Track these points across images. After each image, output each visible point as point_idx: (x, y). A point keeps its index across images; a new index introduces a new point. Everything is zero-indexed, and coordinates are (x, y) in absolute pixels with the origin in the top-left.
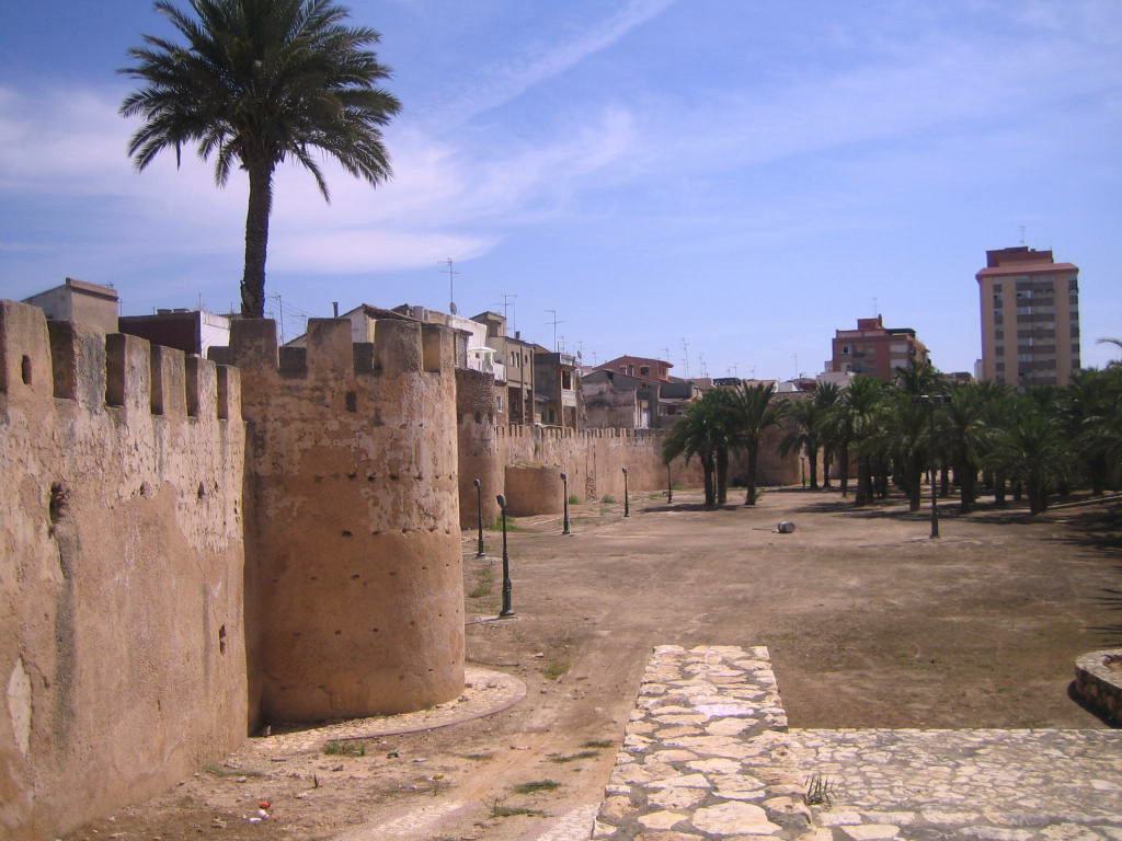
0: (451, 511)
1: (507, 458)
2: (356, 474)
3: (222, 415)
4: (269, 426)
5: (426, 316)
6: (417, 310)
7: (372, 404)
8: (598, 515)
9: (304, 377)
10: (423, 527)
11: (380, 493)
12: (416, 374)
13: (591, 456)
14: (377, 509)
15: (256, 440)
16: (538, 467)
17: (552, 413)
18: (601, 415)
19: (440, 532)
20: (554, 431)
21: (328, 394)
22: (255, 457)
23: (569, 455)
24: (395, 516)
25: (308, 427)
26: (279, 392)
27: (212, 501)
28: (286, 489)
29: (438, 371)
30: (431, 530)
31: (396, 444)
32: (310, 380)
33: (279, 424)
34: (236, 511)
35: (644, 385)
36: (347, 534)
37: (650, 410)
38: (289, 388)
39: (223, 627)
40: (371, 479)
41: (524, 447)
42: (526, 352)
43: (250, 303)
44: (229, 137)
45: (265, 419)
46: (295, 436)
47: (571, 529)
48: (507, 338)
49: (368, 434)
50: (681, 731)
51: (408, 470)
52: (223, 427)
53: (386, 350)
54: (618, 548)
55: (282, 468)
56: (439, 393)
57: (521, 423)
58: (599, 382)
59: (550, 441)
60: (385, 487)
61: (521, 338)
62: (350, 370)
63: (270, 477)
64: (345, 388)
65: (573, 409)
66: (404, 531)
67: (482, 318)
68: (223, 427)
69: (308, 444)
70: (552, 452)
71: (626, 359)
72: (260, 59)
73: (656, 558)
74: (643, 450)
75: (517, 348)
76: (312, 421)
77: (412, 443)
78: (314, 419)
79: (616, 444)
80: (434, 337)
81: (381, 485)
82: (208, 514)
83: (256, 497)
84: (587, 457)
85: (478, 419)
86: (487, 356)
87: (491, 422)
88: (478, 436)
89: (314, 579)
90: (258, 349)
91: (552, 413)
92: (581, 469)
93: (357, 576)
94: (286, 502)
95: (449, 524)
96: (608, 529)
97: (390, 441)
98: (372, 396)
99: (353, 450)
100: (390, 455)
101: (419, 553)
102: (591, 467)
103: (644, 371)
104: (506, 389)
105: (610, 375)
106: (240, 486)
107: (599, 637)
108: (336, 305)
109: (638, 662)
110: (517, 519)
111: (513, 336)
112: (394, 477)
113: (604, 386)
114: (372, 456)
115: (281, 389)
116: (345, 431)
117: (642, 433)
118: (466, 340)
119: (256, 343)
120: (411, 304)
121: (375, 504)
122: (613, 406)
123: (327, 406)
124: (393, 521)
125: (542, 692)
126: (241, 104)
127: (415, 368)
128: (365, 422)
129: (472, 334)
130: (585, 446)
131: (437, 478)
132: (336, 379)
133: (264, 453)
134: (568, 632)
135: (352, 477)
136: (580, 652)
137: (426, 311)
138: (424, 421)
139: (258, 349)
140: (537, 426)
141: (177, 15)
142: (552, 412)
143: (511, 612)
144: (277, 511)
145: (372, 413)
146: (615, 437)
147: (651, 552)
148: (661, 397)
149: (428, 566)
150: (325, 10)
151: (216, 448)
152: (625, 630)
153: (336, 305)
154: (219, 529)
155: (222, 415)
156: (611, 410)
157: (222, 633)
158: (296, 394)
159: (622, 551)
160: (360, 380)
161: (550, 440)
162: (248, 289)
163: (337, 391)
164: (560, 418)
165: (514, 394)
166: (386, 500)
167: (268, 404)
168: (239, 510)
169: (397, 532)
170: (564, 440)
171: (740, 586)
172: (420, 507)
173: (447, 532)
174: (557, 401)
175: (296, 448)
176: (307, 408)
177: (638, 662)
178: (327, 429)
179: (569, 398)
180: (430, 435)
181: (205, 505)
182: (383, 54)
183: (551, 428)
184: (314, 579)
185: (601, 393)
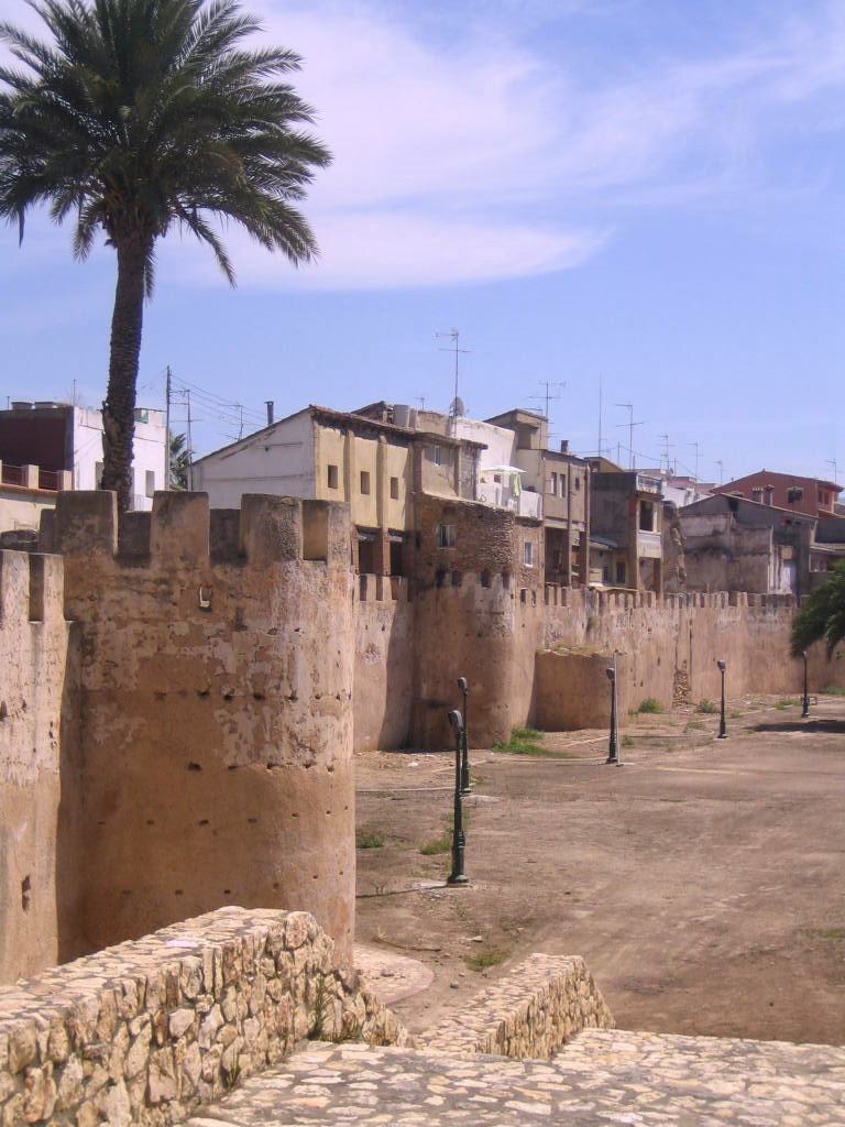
0: (336, 741)
1: (539, 639)
2: (210, 691)
3: (36, 615)
4: (101, 626)
5: (412, 423)
6: (399, 409)
7: (232, 603)
8: (677, 732)
9: (146, 566)
10: (295, 762)
11: (239, 717)
12: (292, 563)
13: (685, 636)
14: (234, 737)
15: (82, 642)
16: (587, 654)
17: (621, 568)
18: (715, 569)
19: (318, 769)
20: (621, 596)
21: (177, 588)
22: (82, 665)
23: (646, 635)
24: (259, 743)
25: (150, 630)
26: (114, 584)
27: (17, 724)
28: (119, 708)
29: (324, 559)
30: (307, 766)
31: (262, 654)
32: (154, 570)
33: (113, 625)
34: (51, 735)
35: (788, 522)
36: (196, 767)
37: (795, 562)
38: (126, 578)
39: (27, 879)
40: (228, 698)
41: (569, 622)
42: (577, 472)
43: (114, 434)
44: (89, 201)
45: (96, 618)
46: (133, 641)
47: (620, 754)
48: (545, 453)
49: (225, 641)
50: (139, 952)
51: (278, 688)
52: (36, 632)
53: (253, 532)
54: (672, 788)
55: (114, 680)
56: (324, 588)
57: (564, 584)
58: (712, 514)
59: (613, 612)
60: (246, 710)
61: (571, 450)
62: (205, 559)
63: (101, 691)
65: (657, 561)
66: (269, 767)
67: (507, 420)
68: (36, 632)
69: (148, 651)
70: (616, 630)
71: (764, 477)
72: (129, 104)
73: (718, 807)
74: (776, 628)
75: (561, 467)
76: (155, 622)
77: (284, 654)
78: (158, 620)
79: (730, 619)
80: (320, 515)
81: (242, 707)
82: (11, 740)
83: (82, 716)
84: (677, 639)
85: (486, 582)
86: (512, 478)
87: (506, 585)
88: (483, 607)
89: (150, 823)
90: (90, 529)
91: (621, 568)
92: (668, 658)
93: (205, 822)
94: (120, 724)
95: (334, 759)
96: (682, 756)
97: (255, 649)
98: (233, 592)
99: (206, 661)
100: (254, 668)
101: (289, 796)
102: (683, 655)
103: (793, 498)
104: (540, 531)
105: (733, 504)
106: (58, 703)
107: (573, 919)
108: (270, 406)
109: (607, 955)
110: (547, 734)
111: (557, 448)
112: (259, 697)
113: (721, 522)
114: (231, 669)
115: (117, 579)
116: (197, 636)
117: (777, 601)
118: (475, 456)
119: (88, 522)
120: (390, 402)
121: (233, 731)
122: (733, 554)
123: (175, 604)
124: (256, 753)
125: (452, 987)
126: (102, 164)
127: (291, 555)
128: (222, 625)
129: (485, 447)
130: (675, 622)
131: (317, 698)
132: (187, 570)
133: (93, 661)
134: (532, 911)
135: (205, 694)
136: (536, 937)
137: (412, 411)
138: (302, 624)
139: (90, 529)
140: (592, 589)
141: (21, 39)
142: (621, 567)
143: (462, 877)
144: (107, 735)
145: (232, 615)
146: (728, 608)
147: (723, 798)
148: (818, 540)
149: (301, 814)
150: (224, 25)
151: (25, 658)
152: (613, 912)
153: (270, 406)
154: (26, 757)
155: (36, 615)
156: (732, 561)
157: (26, 885)
158: (135, 587)
159: (679, 793)
160: (218, 572)
161: (614, 611)
162: (111, 415)
163: (187, 585)
164: (633, 578)
165: (555, 539)
166: (246, 725)
167: (100, 599)
168: (56, 733)
169: (260, 767)
170: (639, 611)
171: (820, 856)
172: (293, 736)
173: (330, 769)
174: (627, 549)
175: (134, 658)
176: (149, 605)
177: (607, 955)
178: (173, 633)
179: (649, 544)
180: (309, 643)
181: (7, 729)
182: (299, 83)
183: (617, 592)
184: (150, 823)
185: (716, 533)
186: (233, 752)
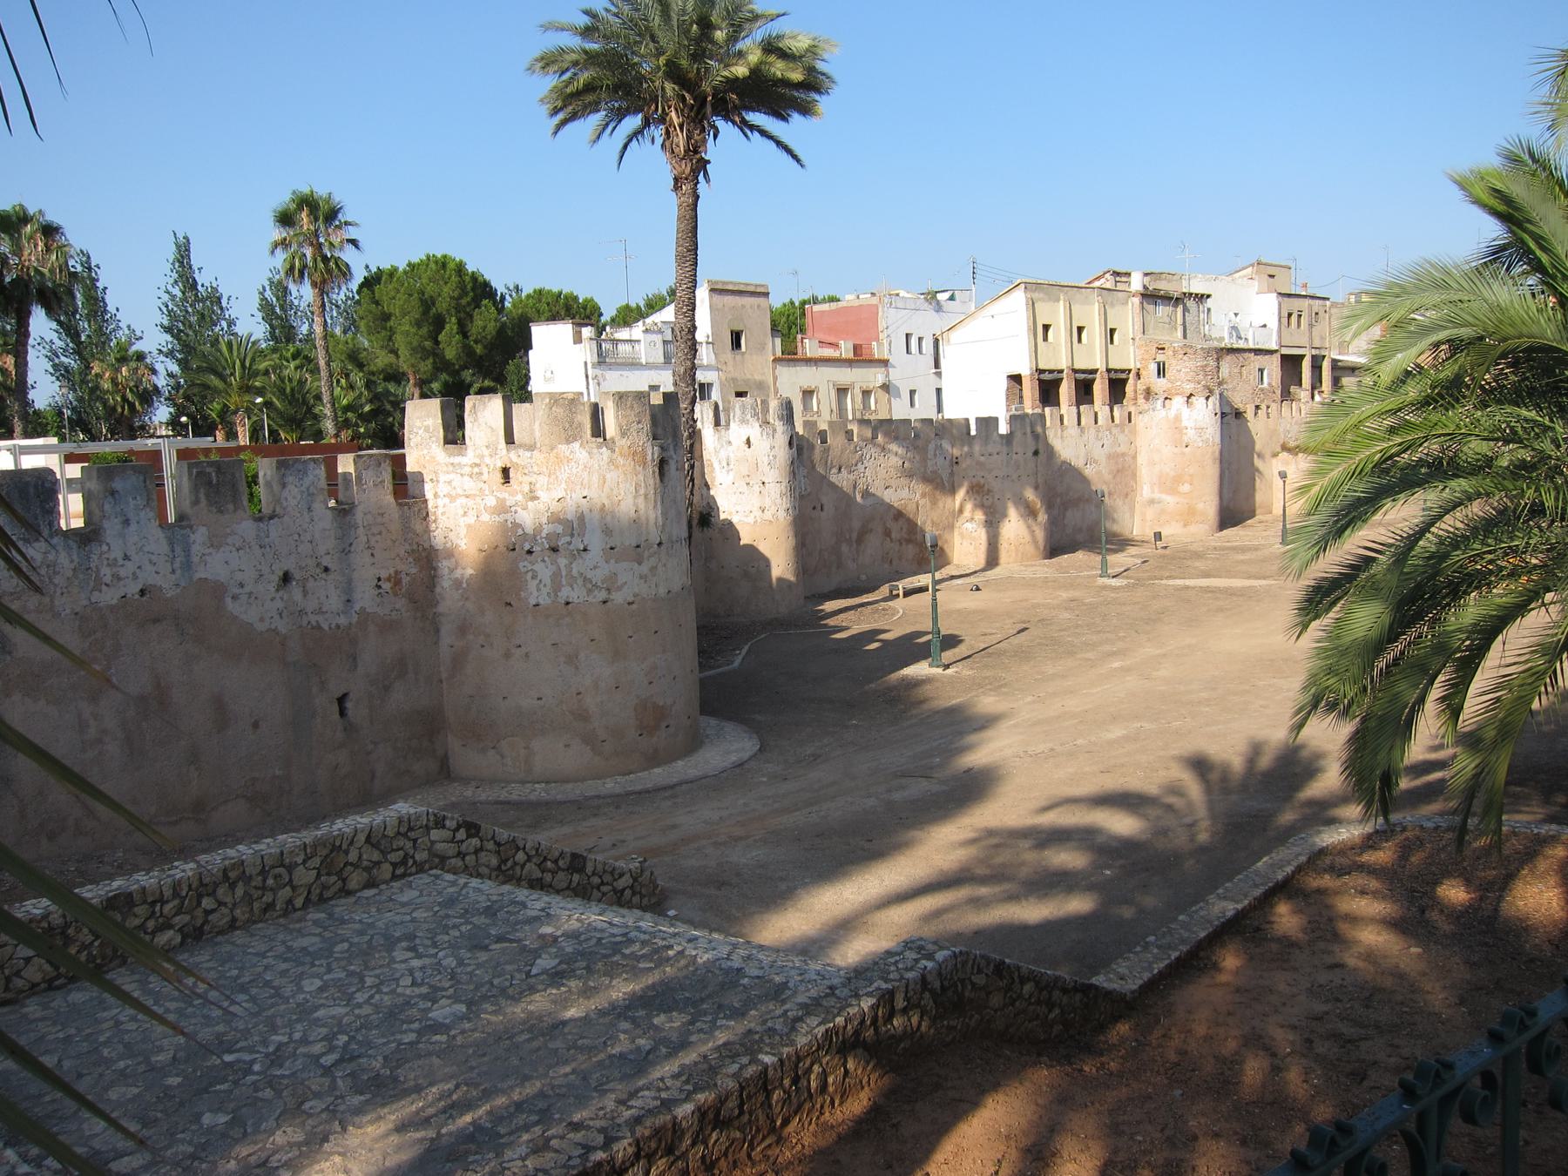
14: (536, 582)
25: (471, 503)
46: (461, 512)
64: (500, 464)
69: (471, 519)
145: (526, 489)
176: (470, 485)
186: (535, 594)
